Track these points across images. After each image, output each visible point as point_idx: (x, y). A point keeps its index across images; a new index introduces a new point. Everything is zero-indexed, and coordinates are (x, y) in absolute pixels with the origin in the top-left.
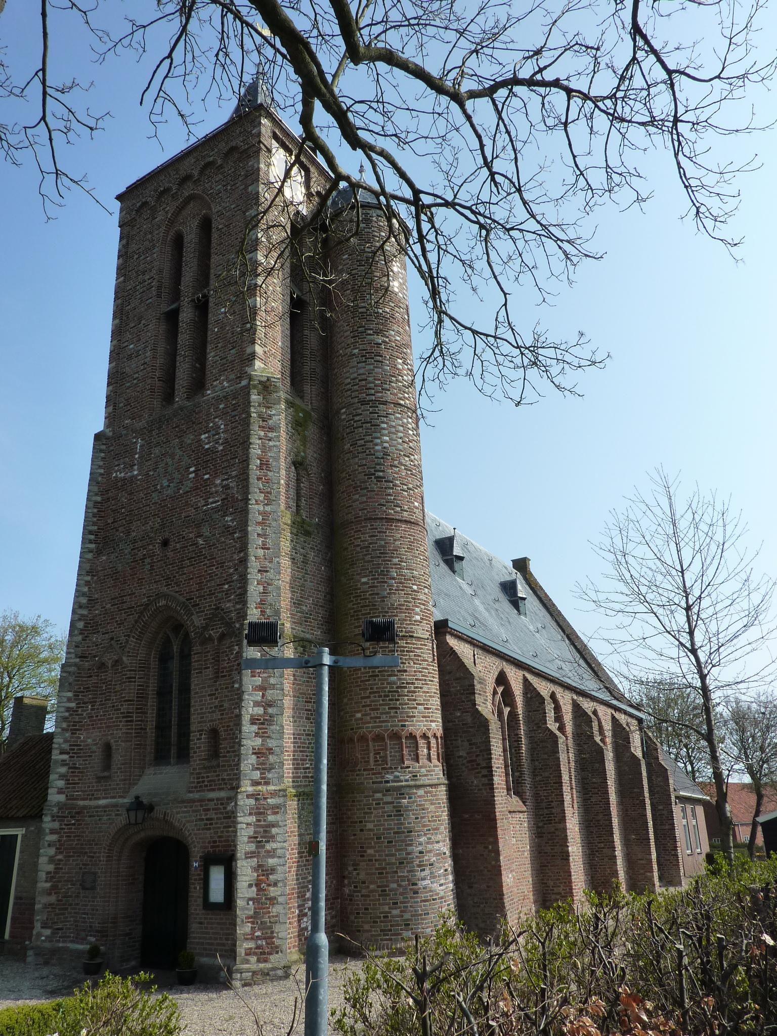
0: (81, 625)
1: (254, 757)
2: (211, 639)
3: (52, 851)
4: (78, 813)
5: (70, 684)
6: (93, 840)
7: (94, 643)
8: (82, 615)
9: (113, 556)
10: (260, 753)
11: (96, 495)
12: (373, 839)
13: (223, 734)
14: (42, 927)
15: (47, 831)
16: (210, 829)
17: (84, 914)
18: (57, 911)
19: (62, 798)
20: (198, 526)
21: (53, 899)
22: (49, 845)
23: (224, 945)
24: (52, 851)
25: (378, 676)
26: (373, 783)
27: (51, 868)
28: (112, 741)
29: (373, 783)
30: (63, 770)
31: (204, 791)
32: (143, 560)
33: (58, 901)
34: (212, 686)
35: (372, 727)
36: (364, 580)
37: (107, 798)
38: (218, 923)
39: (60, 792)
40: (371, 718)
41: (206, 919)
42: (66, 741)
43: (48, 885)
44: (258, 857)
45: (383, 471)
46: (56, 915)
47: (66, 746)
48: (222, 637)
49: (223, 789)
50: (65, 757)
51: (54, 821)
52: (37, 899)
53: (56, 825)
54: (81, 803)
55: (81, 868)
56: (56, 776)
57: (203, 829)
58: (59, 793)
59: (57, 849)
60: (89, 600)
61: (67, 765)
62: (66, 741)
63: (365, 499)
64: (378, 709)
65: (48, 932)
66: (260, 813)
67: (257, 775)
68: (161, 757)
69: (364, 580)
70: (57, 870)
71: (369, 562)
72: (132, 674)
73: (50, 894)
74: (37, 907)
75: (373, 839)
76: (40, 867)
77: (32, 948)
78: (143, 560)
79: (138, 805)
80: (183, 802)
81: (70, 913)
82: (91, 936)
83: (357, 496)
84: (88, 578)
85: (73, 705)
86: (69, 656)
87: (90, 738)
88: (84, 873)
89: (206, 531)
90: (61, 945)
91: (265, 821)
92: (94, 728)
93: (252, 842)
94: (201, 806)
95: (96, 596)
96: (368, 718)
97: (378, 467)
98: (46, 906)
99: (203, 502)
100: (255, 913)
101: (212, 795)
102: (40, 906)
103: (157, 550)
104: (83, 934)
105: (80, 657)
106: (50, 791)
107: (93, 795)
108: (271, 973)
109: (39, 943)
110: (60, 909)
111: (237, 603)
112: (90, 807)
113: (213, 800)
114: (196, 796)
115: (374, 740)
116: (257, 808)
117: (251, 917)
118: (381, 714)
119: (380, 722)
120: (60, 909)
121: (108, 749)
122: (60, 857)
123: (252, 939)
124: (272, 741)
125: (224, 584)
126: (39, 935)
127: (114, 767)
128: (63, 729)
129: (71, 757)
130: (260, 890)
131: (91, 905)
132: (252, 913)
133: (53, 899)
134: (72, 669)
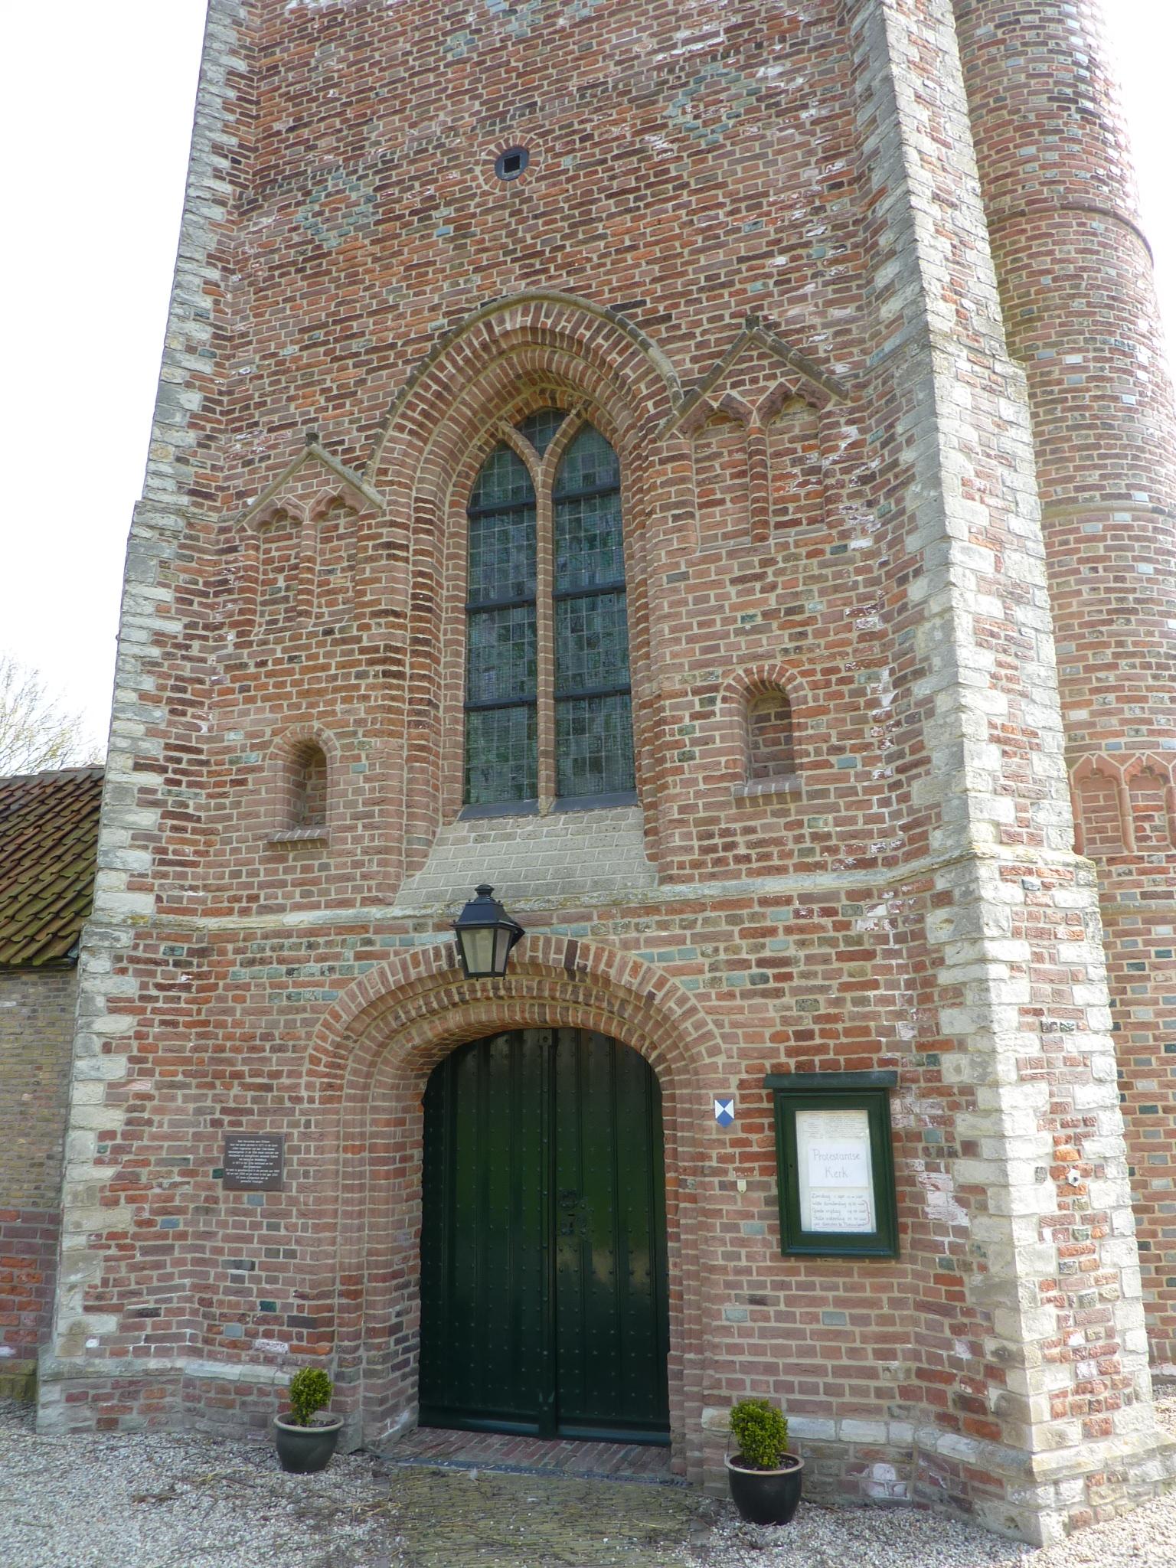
0: (193, 400)
1: (995, 750)
2: (730, 415)
3: (117, 1067)
4: (202, 953)
5: (163, 564)
6: (266, 1037)
7: (237, 456)
8: (196, 374)
9: (300, 213)
10: (1006, 741)
11: (234, 52)
12: (1154, 1050)
13: (803, 693)
14: (87, 1309)
15: (100, 1002)
16: (778, 993)
17: (238, 1265)
18: (138, 1258)
19: (144, 904)
20: (647, 101)
21: (122, 1217)
22: (107, 1049)
23: (872, 1373)
24: (117, 1067)
25: (1134, 611)
26: (1145, 896)
27: (115, 1119)
28: (329, 733)
29: (1145, 896)
30: (148, 818)
31: (737, 875)
32: (423, 213)
33: (140, 1224)
34: (750, 551)
35: (1128, 746)
36: (1075, 359)
37: (316, 906)
38: (840, 1302)
39: (138, 883)
40: (1124, 722)
41: (783, 1286)
42: (152, 732)
43: (108, 1173)
44: (1049, 1077)
45: (1093, 100)
46: (133, 1268)
47: (154, 748)
48: (778, 405)
49: (821, 866)
50: (153, 780)
51: (123, 971)
52: (68, 1219)
53: (129, 986)
54: (212, 923)
55: (216, 1123)
56: (124, 836)
57: (745, 995)
58: (132, 887)
59: (132, 1060)
60: (216, 336)
61: (155, 804)
62: (152, 732)
63: (1054, 156)
64: (1144, 699)
65: (109, 1323)
66: (1040, 934)
67: (1005, 810)
68: (496, 782)
69: (1075, 359)
70: (135, 1126)
71: (1080, 314)
72: (399, 536)
73: (112, 1203)
74: (68, 1243)
75: (1154, 1050)
76: (76, 1116)
77: (56, 1378)
78: (423, 213)
79: (484, 913)
80: (650, 909)
81: (180, 1262)
82: (268, 1335)
83: (1032, 150)
84: (214, 274)
85: (175, 627)
86: (156, 482)
87: (248, 731)
88: (230, 1139)
89: (677, 111)
90: (153, 1364)
91: (1052, 959)
92: (251, 700)
93: (1031, 1028)
94: (733, 920)
95: (241, 327)
96: (1114, 721)
97: (1082, 87)
98: (103, 1240)
99: (652, 44)
100: (1060, 1267)
101: (773, 886)
102: (81, 1240)
103: (481, 179)
104: (237, 1330)
105: (192, 493)
106: (102, 878)
107: (253, 898)
108: (1132, 1472)
109: (79, 1360)
110: (145, 1251)
111: (830, 303)
112: (249, 936)
113: (788, 901)
114: (712, 890)
115: (1134, 780)
116: (1031, 916)
117: (1055, 1284)
118: (1152, 711)
119: (1151, 733)
120: (145, 1251)
121: (309, 759)
122: (144, 1086)
123: (1063, 1359)
124: (1032, 708)
125: (770, 254)
126: (78, 1333)
127: (338, 811)
128: (144, 696)
129: (169, 782)
130: (1067, 1189)
131: (263, 1240)
132: (1051, 1268)
133: (122, 1217)
134: (170, 521)
